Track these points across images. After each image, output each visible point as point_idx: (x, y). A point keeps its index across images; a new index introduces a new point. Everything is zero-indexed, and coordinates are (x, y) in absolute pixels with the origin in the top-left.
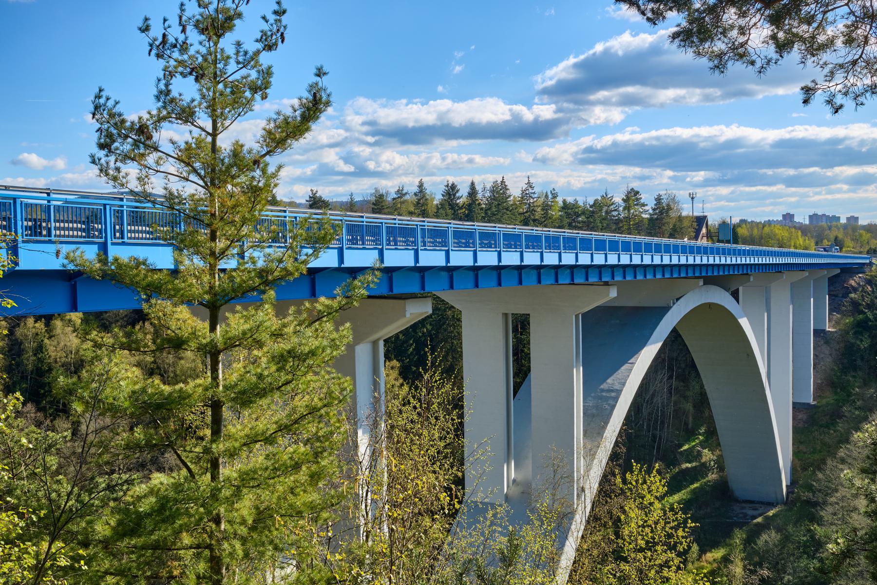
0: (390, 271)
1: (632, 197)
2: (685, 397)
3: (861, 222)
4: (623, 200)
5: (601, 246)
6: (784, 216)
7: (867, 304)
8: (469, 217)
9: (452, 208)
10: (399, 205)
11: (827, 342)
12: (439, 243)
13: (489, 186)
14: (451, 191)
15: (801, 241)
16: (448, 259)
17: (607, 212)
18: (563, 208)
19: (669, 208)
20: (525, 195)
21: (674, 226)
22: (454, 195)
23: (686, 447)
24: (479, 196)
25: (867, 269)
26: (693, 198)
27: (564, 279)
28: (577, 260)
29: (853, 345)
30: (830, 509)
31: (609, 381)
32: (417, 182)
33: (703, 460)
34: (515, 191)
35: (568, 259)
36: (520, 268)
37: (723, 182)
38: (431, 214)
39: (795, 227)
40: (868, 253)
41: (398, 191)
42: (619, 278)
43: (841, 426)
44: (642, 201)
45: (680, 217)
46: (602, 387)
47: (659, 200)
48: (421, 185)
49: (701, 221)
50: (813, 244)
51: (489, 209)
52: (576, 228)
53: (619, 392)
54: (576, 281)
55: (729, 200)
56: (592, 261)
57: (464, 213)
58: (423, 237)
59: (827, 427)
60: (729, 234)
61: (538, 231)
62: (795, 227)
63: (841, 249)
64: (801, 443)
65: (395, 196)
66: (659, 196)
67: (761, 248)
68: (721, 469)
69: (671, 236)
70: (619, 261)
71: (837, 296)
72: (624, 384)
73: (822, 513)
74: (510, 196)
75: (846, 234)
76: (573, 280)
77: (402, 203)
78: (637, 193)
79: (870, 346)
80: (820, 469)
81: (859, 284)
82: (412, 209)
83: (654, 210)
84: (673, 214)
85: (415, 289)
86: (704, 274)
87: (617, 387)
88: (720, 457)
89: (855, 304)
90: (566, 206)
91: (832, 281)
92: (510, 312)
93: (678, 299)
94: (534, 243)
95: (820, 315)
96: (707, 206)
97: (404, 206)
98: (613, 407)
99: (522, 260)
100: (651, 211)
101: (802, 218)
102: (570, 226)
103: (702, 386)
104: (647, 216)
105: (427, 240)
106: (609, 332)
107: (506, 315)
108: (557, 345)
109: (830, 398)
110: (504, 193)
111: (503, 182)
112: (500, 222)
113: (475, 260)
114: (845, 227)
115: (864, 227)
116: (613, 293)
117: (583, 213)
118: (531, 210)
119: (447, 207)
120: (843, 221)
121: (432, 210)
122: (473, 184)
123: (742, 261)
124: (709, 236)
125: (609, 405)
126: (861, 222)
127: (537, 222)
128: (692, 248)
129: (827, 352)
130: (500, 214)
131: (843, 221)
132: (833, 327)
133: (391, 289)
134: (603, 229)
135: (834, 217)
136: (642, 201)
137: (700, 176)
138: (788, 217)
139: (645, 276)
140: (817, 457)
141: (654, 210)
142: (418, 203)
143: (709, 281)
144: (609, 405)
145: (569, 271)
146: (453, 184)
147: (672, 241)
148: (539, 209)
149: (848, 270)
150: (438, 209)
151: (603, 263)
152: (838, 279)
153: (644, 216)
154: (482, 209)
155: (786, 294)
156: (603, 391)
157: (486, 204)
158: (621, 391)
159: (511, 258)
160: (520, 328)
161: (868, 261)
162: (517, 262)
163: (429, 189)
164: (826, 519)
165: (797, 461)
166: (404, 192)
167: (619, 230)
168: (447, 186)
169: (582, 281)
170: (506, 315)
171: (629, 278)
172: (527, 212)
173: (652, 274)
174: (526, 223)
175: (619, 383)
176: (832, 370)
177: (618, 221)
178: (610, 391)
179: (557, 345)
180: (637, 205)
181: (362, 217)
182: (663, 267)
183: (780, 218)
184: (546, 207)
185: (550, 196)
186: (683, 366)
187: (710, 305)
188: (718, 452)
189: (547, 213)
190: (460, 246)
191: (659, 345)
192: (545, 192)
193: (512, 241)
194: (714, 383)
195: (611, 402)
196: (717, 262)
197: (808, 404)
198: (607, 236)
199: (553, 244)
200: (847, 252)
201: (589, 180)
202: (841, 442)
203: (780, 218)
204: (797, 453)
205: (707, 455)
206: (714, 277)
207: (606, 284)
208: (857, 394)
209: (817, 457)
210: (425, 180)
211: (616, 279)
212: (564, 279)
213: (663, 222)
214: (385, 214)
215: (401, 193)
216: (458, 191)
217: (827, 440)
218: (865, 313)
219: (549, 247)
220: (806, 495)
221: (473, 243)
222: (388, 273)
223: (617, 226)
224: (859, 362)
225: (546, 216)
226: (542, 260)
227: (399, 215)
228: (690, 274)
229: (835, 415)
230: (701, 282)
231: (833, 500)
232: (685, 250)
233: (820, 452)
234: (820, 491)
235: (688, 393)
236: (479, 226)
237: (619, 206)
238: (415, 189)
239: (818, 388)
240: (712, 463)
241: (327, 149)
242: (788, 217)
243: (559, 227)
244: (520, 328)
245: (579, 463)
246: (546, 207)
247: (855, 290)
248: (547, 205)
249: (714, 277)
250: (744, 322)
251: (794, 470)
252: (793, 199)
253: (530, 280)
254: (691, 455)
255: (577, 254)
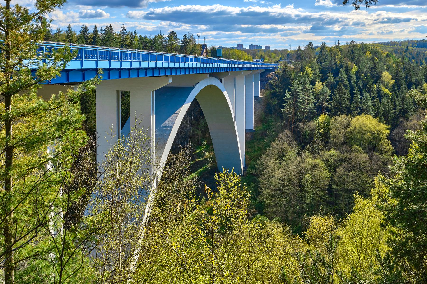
0: (68, 71)
1: (173, 35)
2: (198, 129)
3: (271, 49)
4: (168, 36)
5: (160, 58)
6: (238, 45)
7: (276, 85)
8: (94, 43)
9: (85, 39)
10: (58, 37)
11: (259, 102)
12: (92, 57)
13: (104, 28)
14: (85, 30)
15: (247, 57)
16: (82, 65)
17: (160, 42)
18: (140, 40)
19: (190, 41)
20: (121, 33)
21: (192, 49)
22: (86, 32)
23: (198, 151)
24: (99, 33)
25: (276, 70)
26: (199, 36)
27: (142, 75)
28: (149, 66)
29: (270, 103)
30: (263, 177)
31: (166, 122)
32: (67, 25)
33: (206, 157)
34: (116, 31)
35: (144, 65)
36: (120, 70)
37: (215, 29)
38: (74, 41)
39: (244, 50)
40: (275, 62)
41: (57, 29)
42: (173, 74)
43: (266, 140)
44: (177, 37)
45: (195, 45)
46: (163, 125)
47: (185, 37)
48: (69, 27)
49: (204, 46)
50: (252, 58)
51: (104, 39)
52: (146, 49)
53: (171, 127)
54: (155, 75)
55: (216, 37)
56: (163, 66)
57: (91, 41)
58: (85, 54)
59: (260, 140)
60: (215, 53)
61: (129, 51)
62: (244, 50)
63: (263, 60)
64: (249, 148)
65: (56, 32)
66: (185, 35)
67: (231, 60)
68: (214, 161)
69: (191, 54)
70: (169, 66)
71: (263, 81)
72: (174, 124)
73: (260, 179)
74: (114, 33)
75: (265, 54)
76: (153, 75)
77: (59, 35)
78: (175, 33)
79: (277, 103)
80: (259, 160)
81: (272, 76)
82: (64, 39)
83: (183, 41)
84: (191, 44)
85: (79, 80)
86: (210, 72)
87: (170, 125)
88: (214, 155)
89: (271, 85)
90: (141, 39)
91: (261, 75)
92: (120, 90)
93: (197, 83)
94: (127, 57)
95: (257, 90)
96: (207, 40)
97: (60, 37)
98: (169, 134)
99: (131, 66)
100: (181, 42)
101: (246, 46)
102: (143, 48)
103: (206, 123)
104: (180, 44)
105: (86, 55)
106: (167, 99)
107: (118, 91)
108: (143, 104)
109: (260, 127)
110: (111, 32)
111: (110, 26)
112: (109, 45)
113: (110, 66)
114: (264, 51)
115: (272, 51)
116: (170, 81)
117: (150, 42)
118: (124, 40)
119: (83, 38)
120: (263, 48)
121: (75, 39)
122: (96, 27)
123: (223, 65)
124: (207, 54)
125: (167, 134)
126: (271, 49)
127: (127, 46)
128: (199, 59)
129: (259, 107)
130: (109, 42)
131: (263, 48)
132: (262, 95)
133: (68, 80)
134: (160, 50)
135: (260, 46)
136: (177, 37)
137: (203, 27)
138: (240, 46)
139: (185, 73)
140: (256, 154)
141: (183, 41)
142: (68, 36)
143: (211, 75)
144: (167, 134)
145: (151, 70)
146: (86, 27)
147: (190, 56)
148: (128, 40)
149: (268, 70)
150: (78, 39)
151: (161, 67)
152: (264, 74)
153: (178, 44)
154: (100, 39)
155: (243, 81)
156: (164, 127)
157: (102, 37)
158: (173, 127)
159: (126, 65)
160: (124, 97)
161: (276, 66)
162: (119, 67)
163: (73, 29)
164: (261, 182)
165: (247, 156)
166: (60, 30)
167: (166, 51)
168: (83, 28)
169: (158, 75)
170: (118, 91)
171: (178, 74)
172: (122, 41)
173: (164, 72)
174: (122, 46)
175: (171, 123)
176: (262, 114)
177: (166, 46)
178: (167, 127)
179: (143, 104)
180: (175, 39)
181: (54, 44)
182: (189, 68)
183: (237, 46)
184: (132, 39)
185: (134, 34)
186: (196, 114)
187: (211, 86)
188: (212, 153)
189: (132, 42)
190: (101, 59)
191: (190, 104)
192: (131, 31)
193: (116, 56)
194: (211, 121)
195: (168, 132)
196: (208, 66)
197: (252, 130)
198: (163, 54)
199: (137, 57)
200: (266, 62)
201: (155, 27)
202: (266, 147)
203: (237, 46)
204: (247, 153)
205: (208, 155)
206: (216, 74)
207: (167, 76)
208: (273, 125)
209: (256, 154)
210: (72, 25)
211: (172, 74)
212: (149, 74)
213: (187, 47)
214: (50, 41)
215: (58, 30)
216: (88, 30)
217: (260, 146)
218: (275, 89)
219: (143, 59)
220: (253, 171)
221: (118, 57)
222: (66, 72)
223: (165, 48)
224: (273, 111)
225: (131, 43)
226: (140, 66)
227: (58, 41)
228: (204, 72)
229: (263, 135)
230: (208, 76)
231: (264, 173)
232: (196, 60)
233: (257, 151)
234: (258, 169)
235: (199, 127)
236: (99, 48)
237: (166, 39)
238: (67, 29)
239: (256, 123)
240: (210, 159)
241: (403, 23)
242: (240, 46)
243: (138, 49)
244: (124, 97)
245: (154, 160)
246: (132, 39)
247: (271, 79)
248: (132, 38)
249: (216, 74)
250: (225, 93)
251: (246, 160)
252: (244, 38)
253: (124, 75)
254: (200, 155)
255: (156, 62)
